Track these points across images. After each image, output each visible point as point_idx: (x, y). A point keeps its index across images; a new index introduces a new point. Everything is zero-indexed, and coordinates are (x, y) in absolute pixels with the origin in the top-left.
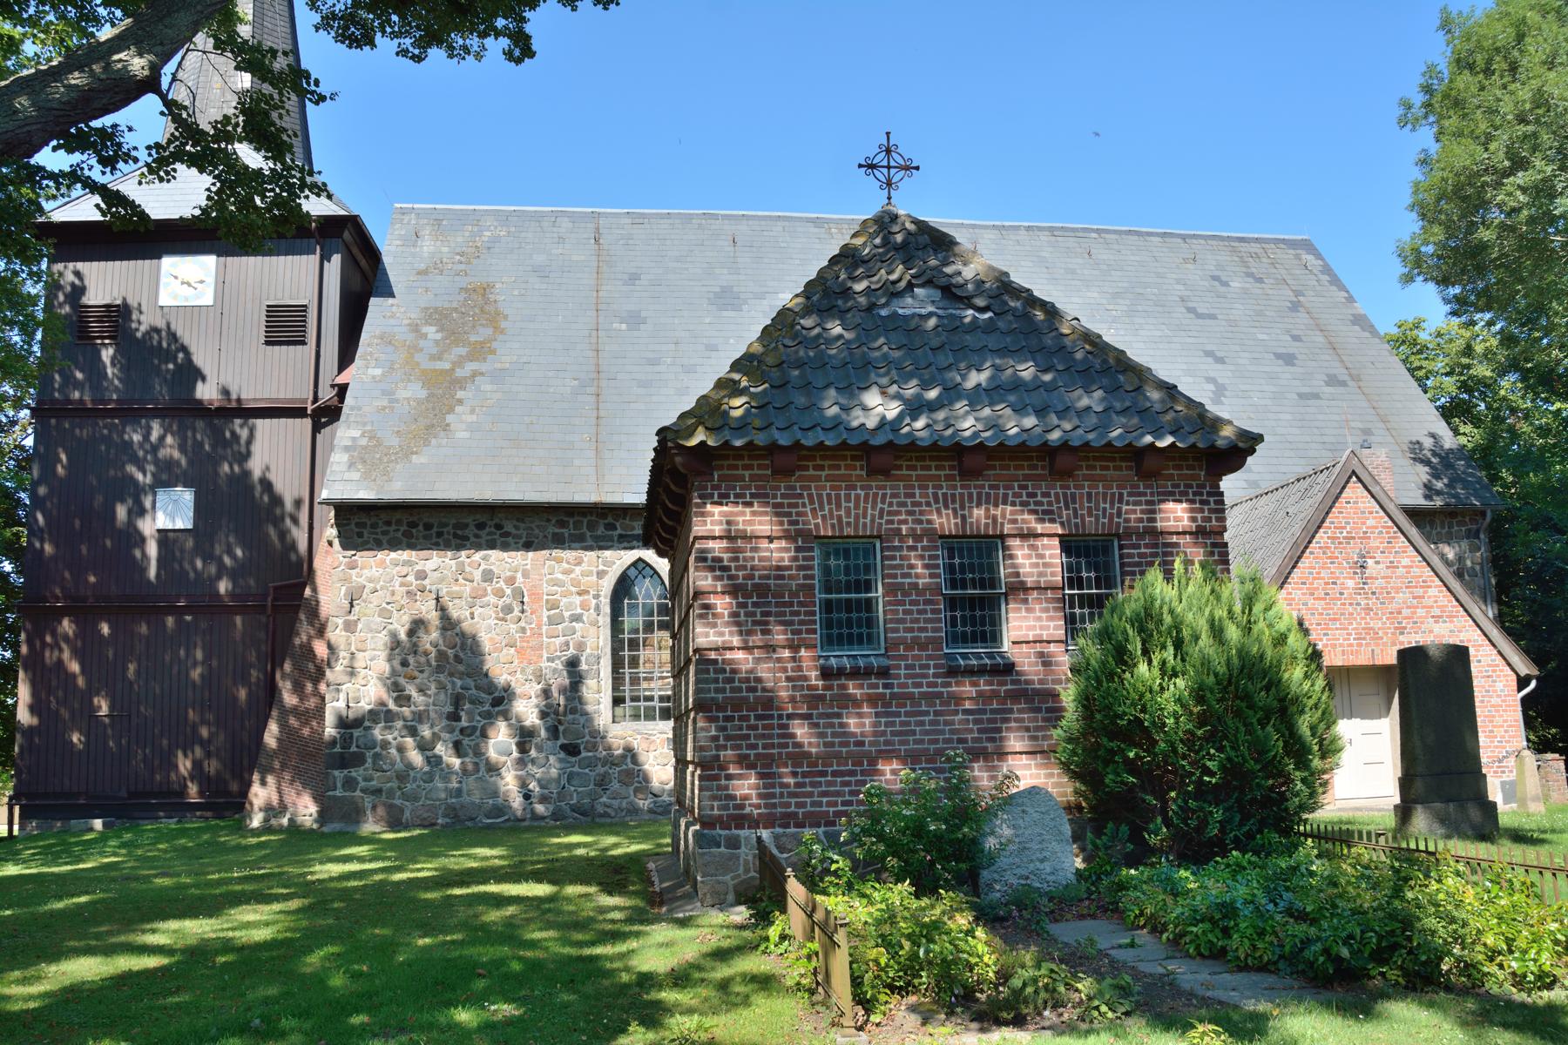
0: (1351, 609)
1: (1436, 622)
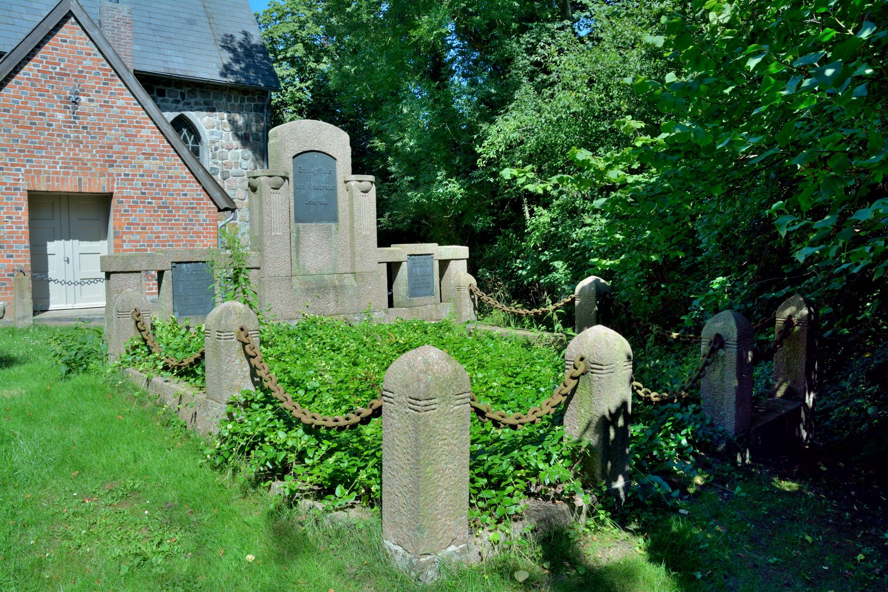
1: (146, 158)
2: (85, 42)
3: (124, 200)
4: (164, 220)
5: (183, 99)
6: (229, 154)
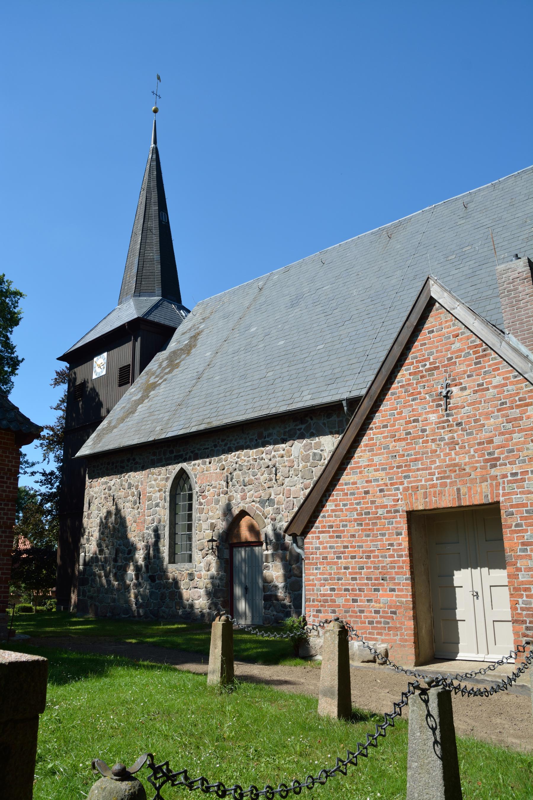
2: (451, 323)
3: (514, 510)
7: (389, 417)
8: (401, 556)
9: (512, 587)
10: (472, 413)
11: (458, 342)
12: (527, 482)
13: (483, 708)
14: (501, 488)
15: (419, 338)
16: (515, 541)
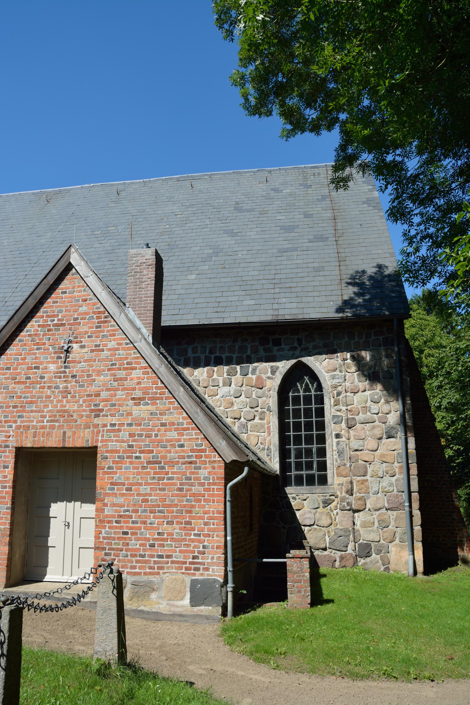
0: (49, 393)
1: (135, 404)
2: (83, 289)
3: (108, 455)
4: (154, 478)
5: (300, 344)
6: (355, 397)
7: (13, 361)
8: (5, 487)
9: (98, 520)
10: (86, 368)
11: (85, 306)
12: (122, 432)
13: (60, 623)
14: (100, 435)
15: (53, 295)
16: (106, 481)
